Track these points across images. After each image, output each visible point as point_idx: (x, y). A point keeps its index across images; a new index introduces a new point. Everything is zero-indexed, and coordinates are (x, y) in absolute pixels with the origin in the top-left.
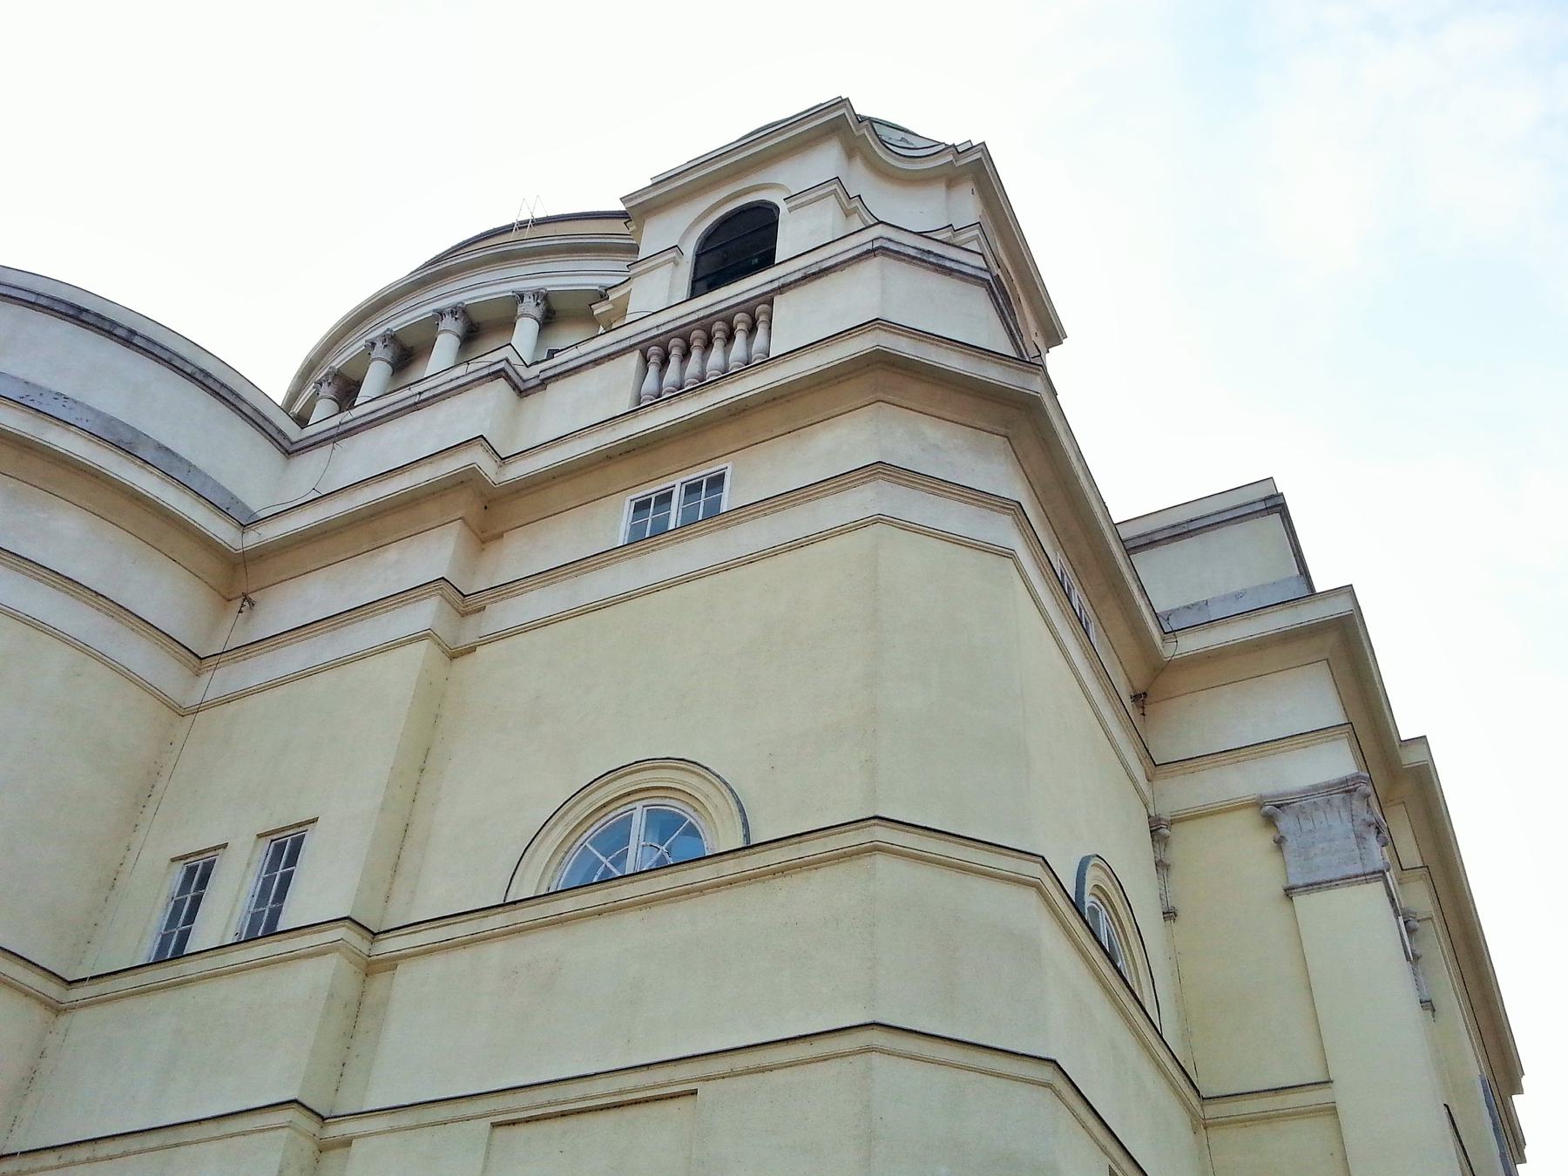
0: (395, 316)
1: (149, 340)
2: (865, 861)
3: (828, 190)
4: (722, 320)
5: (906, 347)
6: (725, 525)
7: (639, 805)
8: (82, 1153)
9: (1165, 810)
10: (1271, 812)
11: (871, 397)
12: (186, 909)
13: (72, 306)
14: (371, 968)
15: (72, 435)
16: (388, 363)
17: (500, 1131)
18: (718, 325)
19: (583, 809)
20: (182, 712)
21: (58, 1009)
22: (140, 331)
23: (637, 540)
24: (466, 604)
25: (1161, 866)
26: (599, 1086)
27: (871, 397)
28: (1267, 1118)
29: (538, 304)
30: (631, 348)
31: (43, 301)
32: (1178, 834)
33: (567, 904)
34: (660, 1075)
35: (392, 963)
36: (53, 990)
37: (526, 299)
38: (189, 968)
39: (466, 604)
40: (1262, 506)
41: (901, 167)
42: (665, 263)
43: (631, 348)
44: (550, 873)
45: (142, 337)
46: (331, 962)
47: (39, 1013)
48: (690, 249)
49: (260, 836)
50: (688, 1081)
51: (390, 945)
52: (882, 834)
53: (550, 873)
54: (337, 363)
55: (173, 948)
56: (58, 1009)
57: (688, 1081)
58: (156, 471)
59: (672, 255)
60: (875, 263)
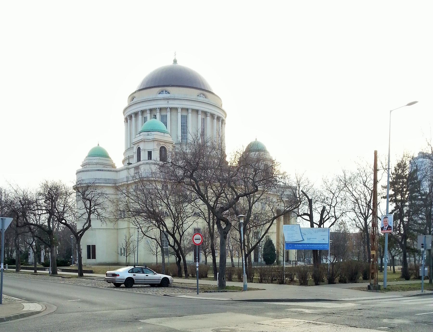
59: (135, 153)
60: (143, 165)
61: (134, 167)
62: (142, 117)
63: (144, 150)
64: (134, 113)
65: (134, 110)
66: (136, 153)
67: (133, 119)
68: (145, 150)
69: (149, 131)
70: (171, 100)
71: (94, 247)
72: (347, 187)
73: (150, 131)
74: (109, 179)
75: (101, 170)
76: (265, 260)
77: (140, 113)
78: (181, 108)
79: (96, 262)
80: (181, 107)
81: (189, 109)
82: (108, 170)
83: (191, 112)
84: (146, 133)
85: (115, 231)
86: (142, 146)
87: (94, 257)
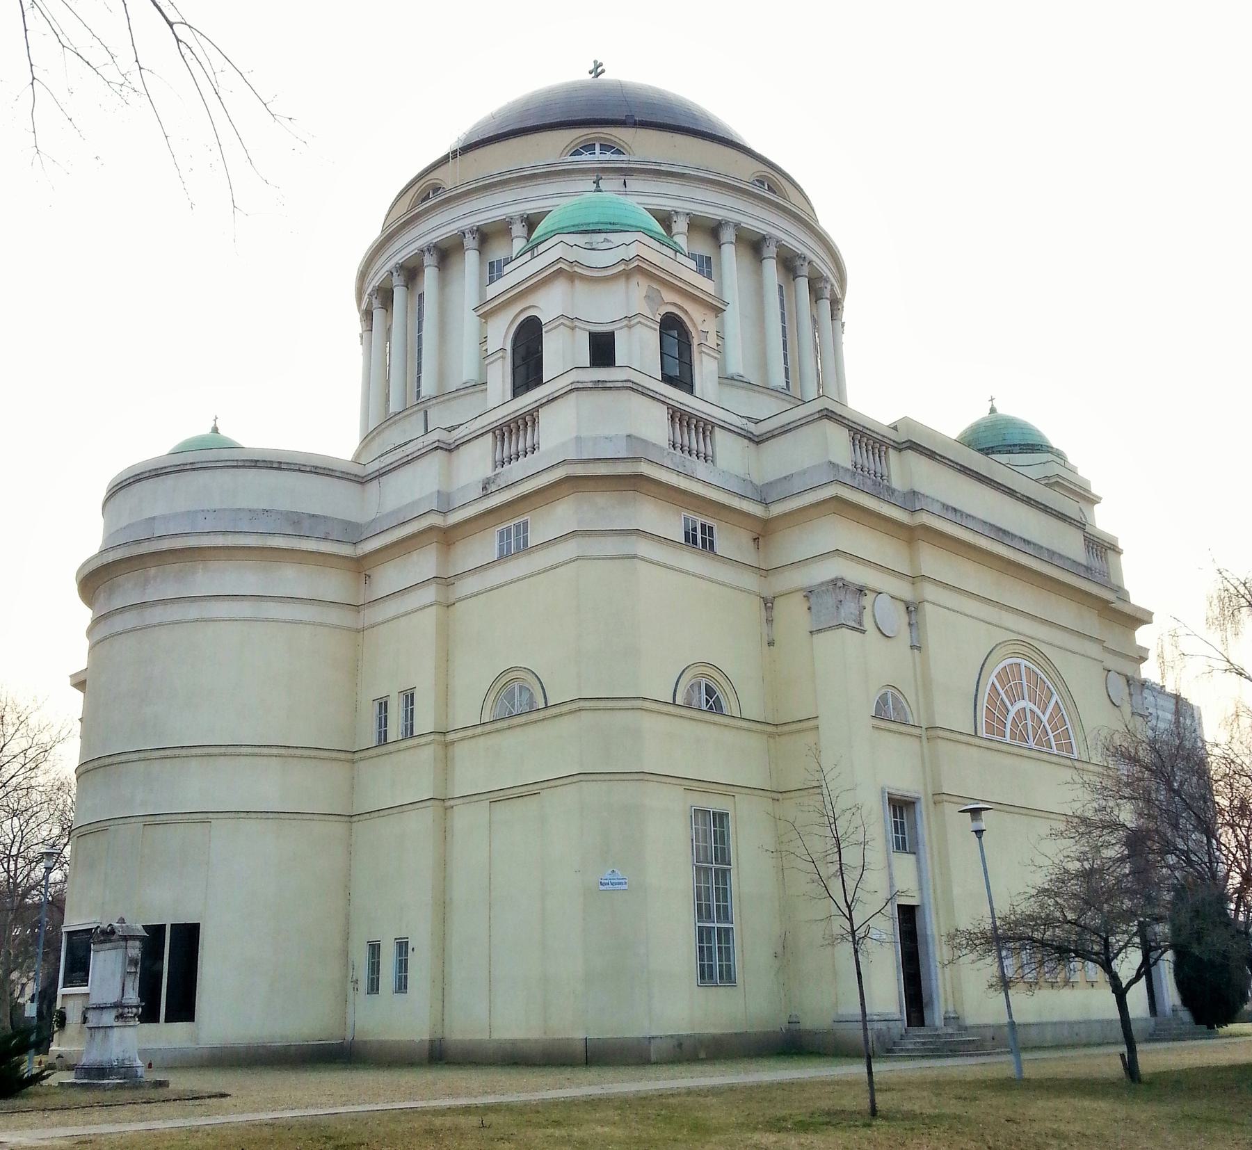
0: (399, 251)
1: (288, 463)
2: (578, 714)
3: (558, 323)
4: (522, 419)
5: (579, 470)
6: (529, 554)
7: (516, 683)
8: (376, 814)
9: (768, 594)
10: (809, 593)
11: (572, 491)
12: (383, 722)
13: (252, 461)
14: (447, 745)
15: (277, 538)
16: (402, 286)
17: (492, 804)
18: (520, 422)
19: (499, 685)
20: (358, 631)
21: (353, 762)
22: (283, 461)
23: (504, 556)
24: (445, 581)
25: (769, 621)
26: (515, 791)
27: (572, 491)
28: (798, 731)
29: (474, 238)
30: (488, 432)
31: (240, 464)
32: (779, 603)
33: (499, 725)
34: (530, 788)
35: (453, 743)
36: (349, 756)
37: (467, 236)
38: (391, 748)
39: (445, 581)
40: (817, 416)
41: (600, 275)
42: (499, 358)
43: (488, 432)
44: (493, 712)
45: (284, 463)
46: (432, 747)
47: (348, 765)
48: (509, 347)
49: (399, 693)
50: (537, 790)
51: (451, 737)
52: (582, 704)
53: (493, 712)
54: (376, 282)
55: (383, 739)
56: (353, 762)
57: (537, 790)
58: (313, 539)
59: (500, 354)
60: (574, 395)
61: (493, 431)
62: (481, 261)
63: (571, 322)
64: (436, 246)
65: (434, 235)
66: (503, 357)
67: (429, 277)
68: (577, 323)
69: (594, 231)
70: (642, 176)
71: (188, 936)
72: (444, 834)
73: (599, 231)
74: (313, 515)
75: (271, 462)
76: (1186, 1001)
77: (470, 242)
78: (688, 214)
79: (193, 1045)
80: (687, 211)
81: (727, 223)
82: (316, 467)
83: (734, 241)
84: (581, 240)
85: (338, 828)
86: (548, 305)
87: (183, 1009)
